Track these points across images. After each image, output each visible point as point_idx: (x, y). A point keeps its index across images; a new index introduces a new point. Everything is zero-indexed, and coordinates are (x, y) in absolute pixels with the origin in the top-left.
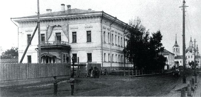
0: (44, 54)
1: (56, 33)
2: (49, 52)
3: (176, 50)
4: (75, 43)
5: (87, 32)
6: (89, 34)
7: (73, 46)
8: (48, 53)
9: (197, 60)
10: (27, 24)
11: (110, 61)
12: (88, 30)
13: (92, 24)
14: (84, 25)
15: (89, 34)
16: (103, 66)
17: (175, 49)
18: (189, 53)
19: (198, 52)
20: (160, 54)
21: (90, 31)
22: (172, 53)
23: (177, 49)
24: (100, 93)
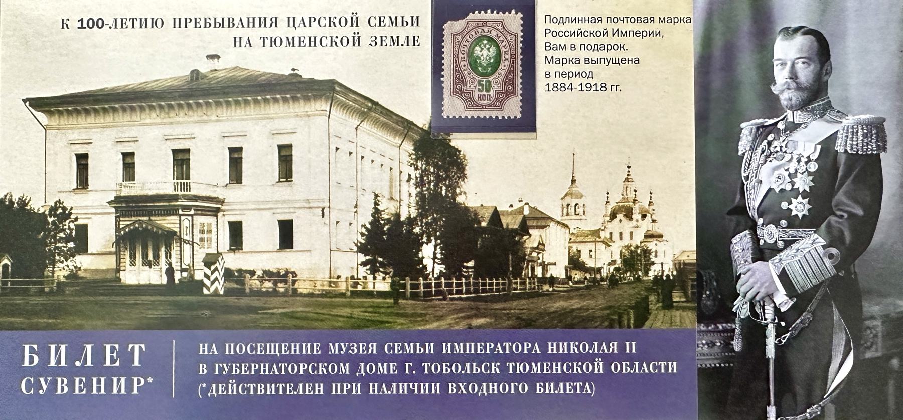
0: (135, 222)
1: (279, 146)
2: (152, 218)
3: (572, 210)
4: (83, 191)
5: (281, 147)
6: (286, 156)
7: (232, 195)
8: (150, 219)
9: (652, 245)
10: (131, 114)
11: (187, 248)
12: (81, 150)
13: (196, 130)
14: (113, 134)
15: (286, 156)
16: (826, 277)
17: (568, 205)
18: (620, 221)
19: (654, 217)
20: (369, 226)
21: (290, 146)
22: (558, 223)
23: (576, 205)
24: (16, 392)
